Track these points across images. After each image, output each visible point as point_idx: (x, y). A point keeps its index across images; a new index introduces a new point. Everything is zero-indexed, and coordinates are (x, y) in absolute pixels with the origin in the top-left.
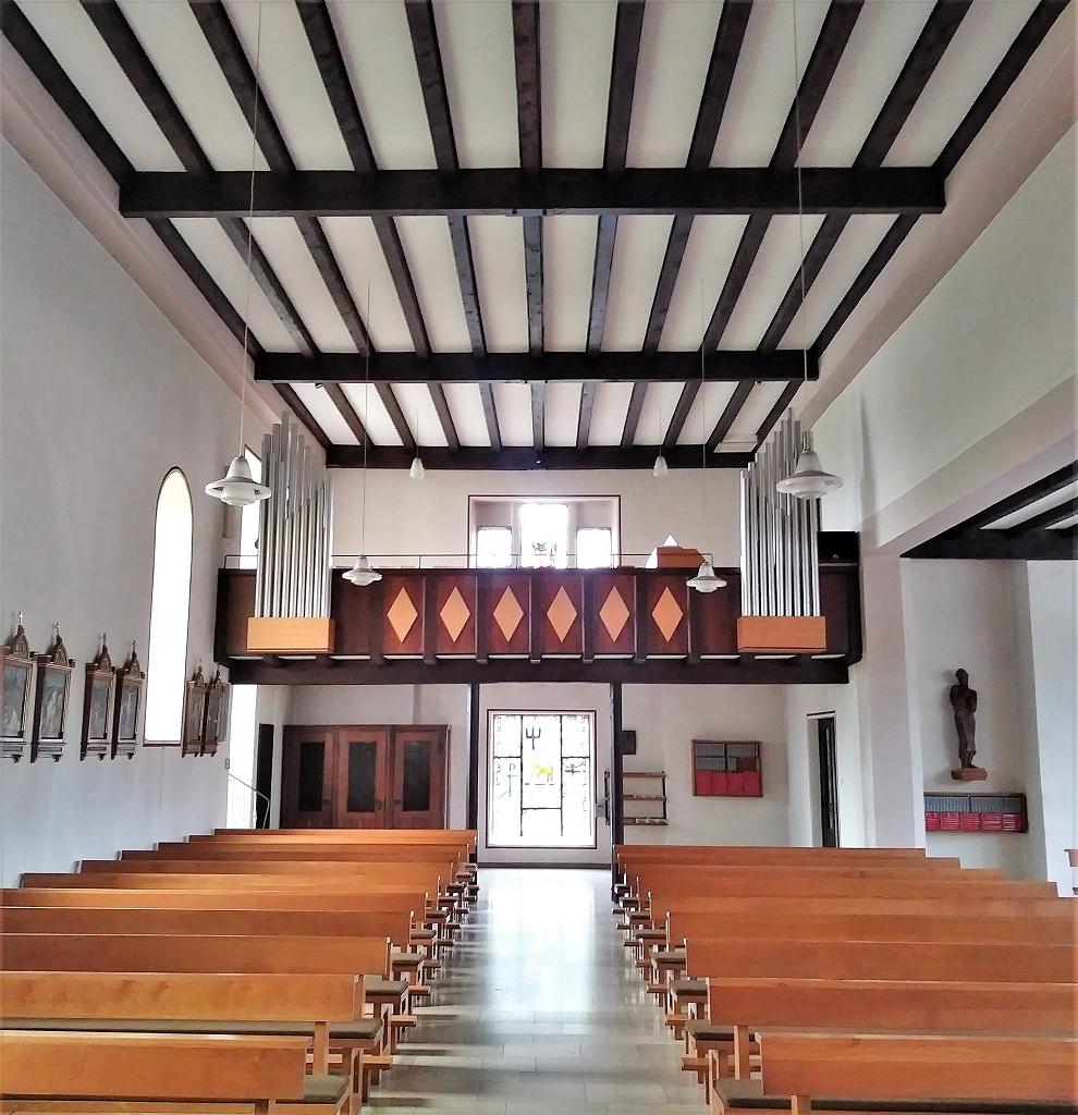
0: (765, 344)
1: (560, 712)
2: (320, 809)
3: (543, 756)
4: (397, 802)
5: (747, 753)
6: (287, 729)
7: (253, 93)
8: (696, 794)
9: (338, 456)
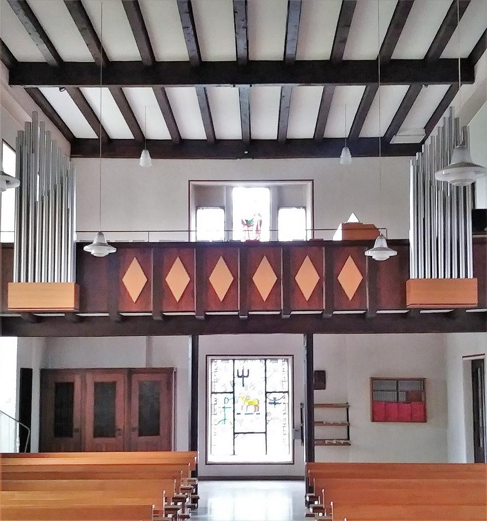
0: (432, 52)
1: (265, 356)
2: (71, 436)
3: (253, 389)
4: (133, 429)
5: (416, 387)
6: (44, 372)
7: (100, 50)
8: (373, 420)
9: (79, 148)
